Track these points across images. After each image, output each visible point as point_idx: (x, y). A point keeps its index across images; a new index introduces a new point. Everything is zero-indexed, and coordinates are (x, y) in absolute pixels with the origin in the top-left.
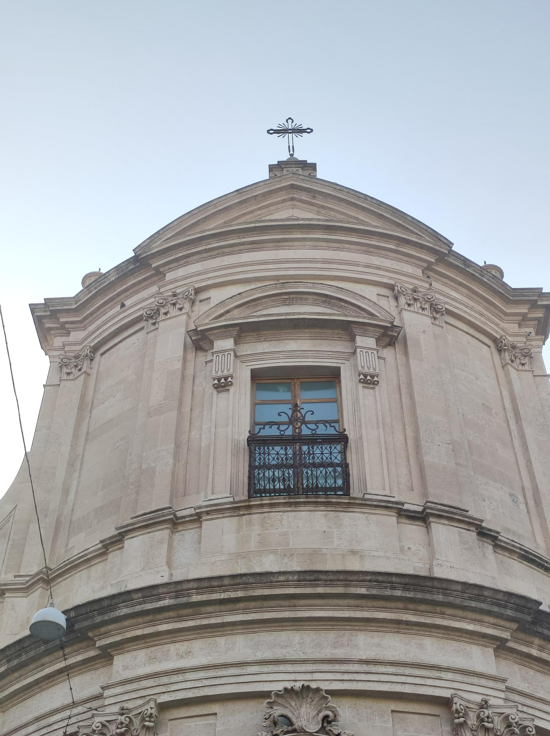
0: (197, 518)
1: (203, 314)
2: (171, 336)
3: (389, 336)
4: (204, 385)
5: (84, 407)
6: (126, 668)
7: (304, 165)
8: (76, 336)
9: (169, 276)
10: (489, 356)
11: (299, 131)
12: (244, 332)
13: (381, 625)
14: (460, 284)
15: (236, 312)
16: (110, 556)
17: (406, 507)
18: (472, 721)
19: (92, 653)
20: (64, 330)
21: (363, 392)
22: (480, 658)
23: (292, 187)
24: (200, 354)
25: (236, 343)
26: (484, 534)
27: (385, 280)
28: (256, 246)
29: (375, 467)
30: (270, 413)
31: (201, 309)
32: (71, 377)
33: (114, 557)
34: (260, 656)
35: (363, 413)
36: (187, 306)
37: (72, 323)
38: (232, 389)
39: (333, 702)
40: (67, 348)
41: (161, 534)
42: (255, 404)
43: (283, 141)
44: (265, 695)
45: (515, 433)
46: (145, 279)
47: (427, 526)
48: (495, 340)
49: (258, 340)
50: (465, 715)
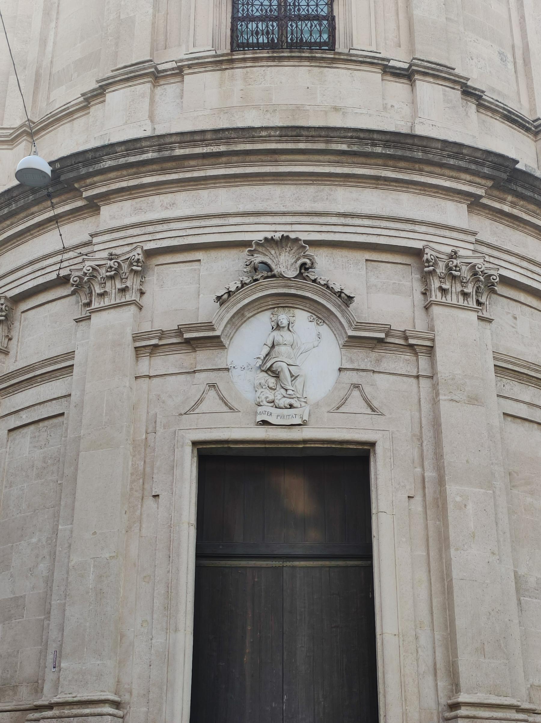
0: (179, 72)
13: (360, 180)
16: (92, 110)
17: (392, 63)
18: (441, 269)
19: (79, 203)
22: (454, 213)
26: (469, 93)
33: (96, 110)
39: (310, 251)
41: (143, 88)
47: (412, 84)
50: (435, 264)
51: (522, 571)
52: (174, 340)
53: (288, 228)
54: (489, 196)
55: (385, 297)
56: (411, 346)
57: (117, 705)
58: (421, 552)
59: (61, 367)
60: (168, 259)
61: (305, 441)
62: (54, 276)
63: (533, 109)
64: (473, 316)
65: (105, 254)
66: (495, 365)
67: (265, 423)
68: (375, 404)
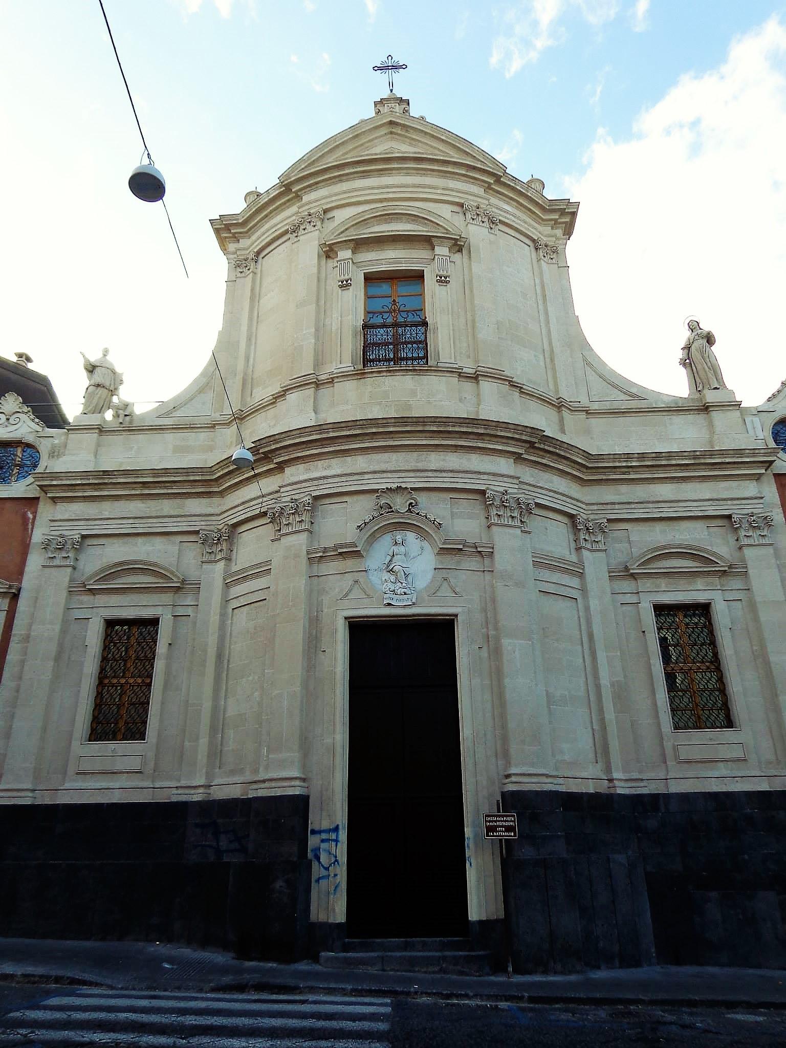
0: (331, 381)
1: (332, 229)
2: (308, 246)
3: (458, 245)
4: (333, 284)
5: (254, 298)
6: (292, 475)
7: (401, 101)
8: (244, 243)
9: (306, 198)
10: (528, 254)
11: (396, 67)
12: (359, 244)
14: (511, 199)
15: (352, 229)
16: (278, 404)
17: (465, 370)
18: (497, 502)
19: (272, 466)
20: (236, 238)
21: (440, 291)
22: (504, 465)
23: (391, 123)
24: (330, 261)
25: (353, 253)
26: (513, 385)
27: (457, 200)
28: (365, 174)
29: (444, 343)
30: (378, 305)
31: (330, 226)
32: (243, 275)
33: (282, 405)
34: (372, 468)
35: (438, 302)
36: (319, 223)
37: (241, 233)
38: (351, 288)
39: (415, 495)
40: (238, 253)
41: (310, 391)
42: (368, 297)
43: (383, 77)
44: (376, 491)
45: (542, 312)
46: (288, 201)
47: (478, 383)
48: (533, 241)
49: (368, 251)
50: (493, 499)
51: (551, 690)
52: (332, 553)
53: (401, 480)
54: (527, 453)
55: (465, 523)
56: (480, 552)
57: (304, 780)
58: (487, 682)
59: (262, 570)
60: (327, 501)
61: (414, 615)
62: (257, 512)
63: (557, 391)
64: (518, 531)
65: (288, 499)
66: (660, 609)
67: (389, 604)
68: (457, 590)
